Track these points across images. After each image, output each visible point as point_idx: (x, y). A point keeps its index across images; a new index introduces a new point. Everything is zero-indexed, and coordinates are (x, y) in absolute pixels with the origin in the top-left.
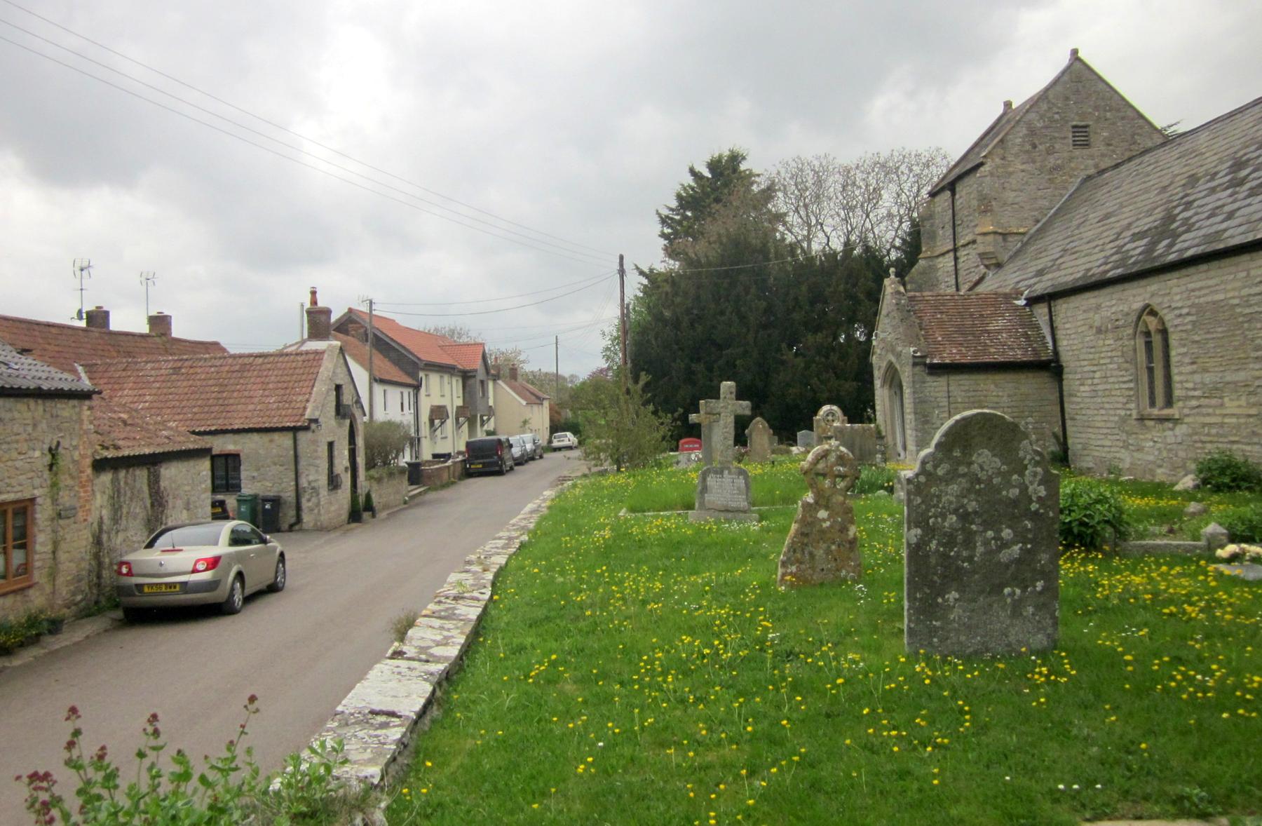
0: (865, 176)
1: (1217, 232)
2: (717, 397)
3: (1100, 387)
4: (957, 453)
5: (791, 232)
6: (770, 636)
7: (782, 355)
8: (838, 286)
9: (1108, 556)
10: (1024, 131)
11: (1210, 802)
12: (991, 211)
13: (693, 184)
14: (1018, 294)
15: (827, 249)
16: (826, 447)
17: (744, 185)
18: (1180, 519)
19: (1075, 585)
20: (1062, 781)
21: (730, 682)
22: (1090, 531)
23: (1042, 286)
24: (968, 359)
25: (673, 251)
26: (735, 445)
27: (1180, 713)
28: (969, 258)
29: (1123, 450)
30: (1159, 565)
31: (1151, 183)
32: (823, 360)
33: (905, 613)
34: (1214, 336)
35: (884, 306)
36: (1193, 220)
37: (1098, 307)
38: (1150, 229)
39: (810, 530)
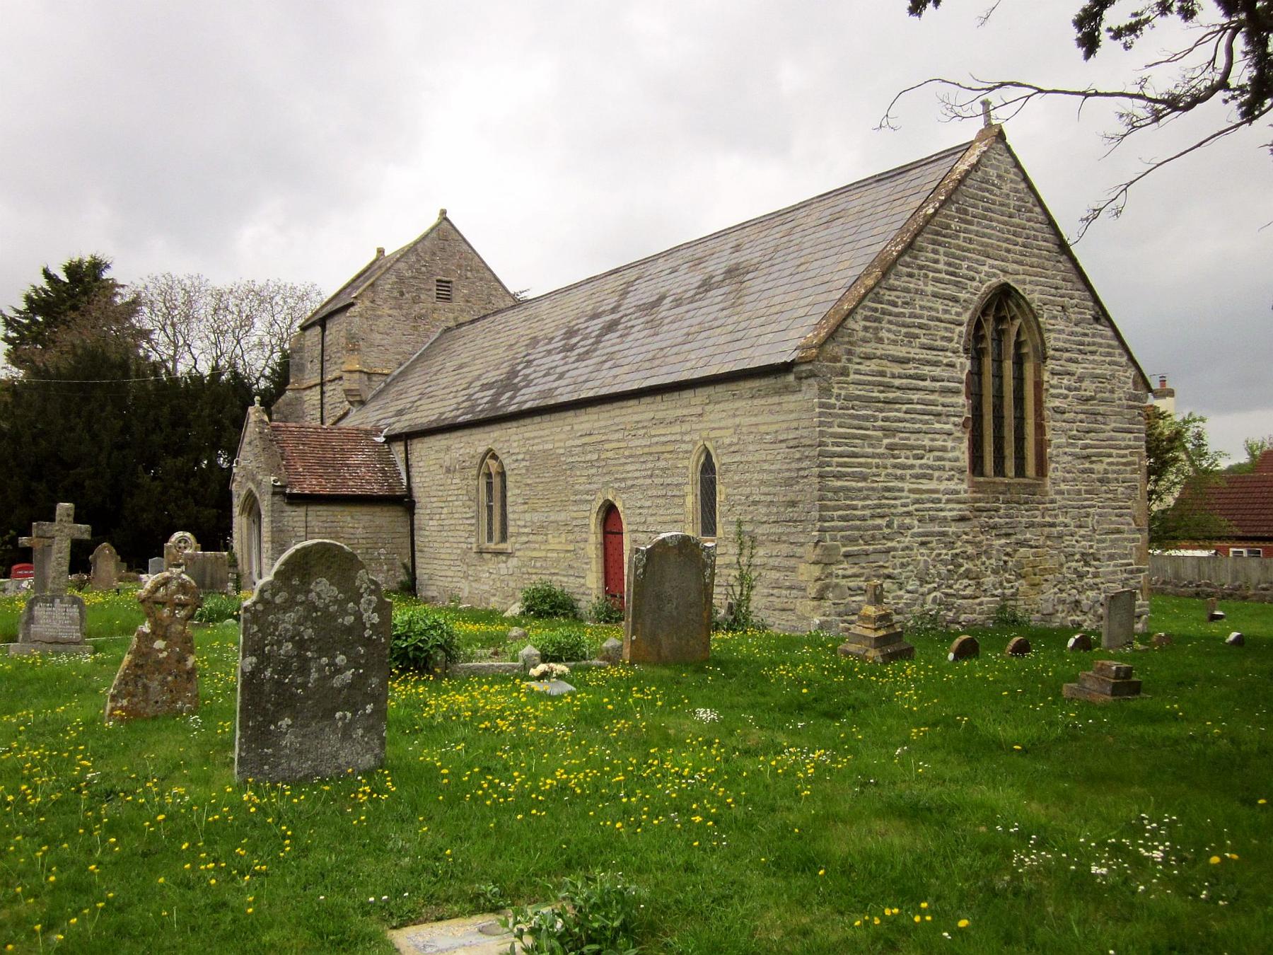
0: (238, 302)
1: (550, 389)
2: (52, 520)
3: (446, 522)
4: (295, 582)
5: (158, 349)
6: (89, 775)
7: (138, 478)
8: (202, 410)
9: (439, 678)
10: (394, 279)
11: (501, 896)
12: (358, 350)
13: (47, 287)
14: (378, 431)
15: (194, 371)
16: (167, 574)
17: (106, 296)
18: (505, 642)
19: (406, 706)
20: (373, 893)
21: (37, 829)
22: (424, 655)
23: (400, 426)
24: (327, 491)
25: (18, 357)
26: (72, 571)
27: (484, 818)
28: (335, 393)
29: (463, 581)
30: (480, 684)
31: (501, 340)
32: (183, 485)
33: (237, 743)
34: (543, 480)
35: (247, 434)
36: (532, 377)
37: (448, 449)
38: (496, 381)
39: (143, 663)
